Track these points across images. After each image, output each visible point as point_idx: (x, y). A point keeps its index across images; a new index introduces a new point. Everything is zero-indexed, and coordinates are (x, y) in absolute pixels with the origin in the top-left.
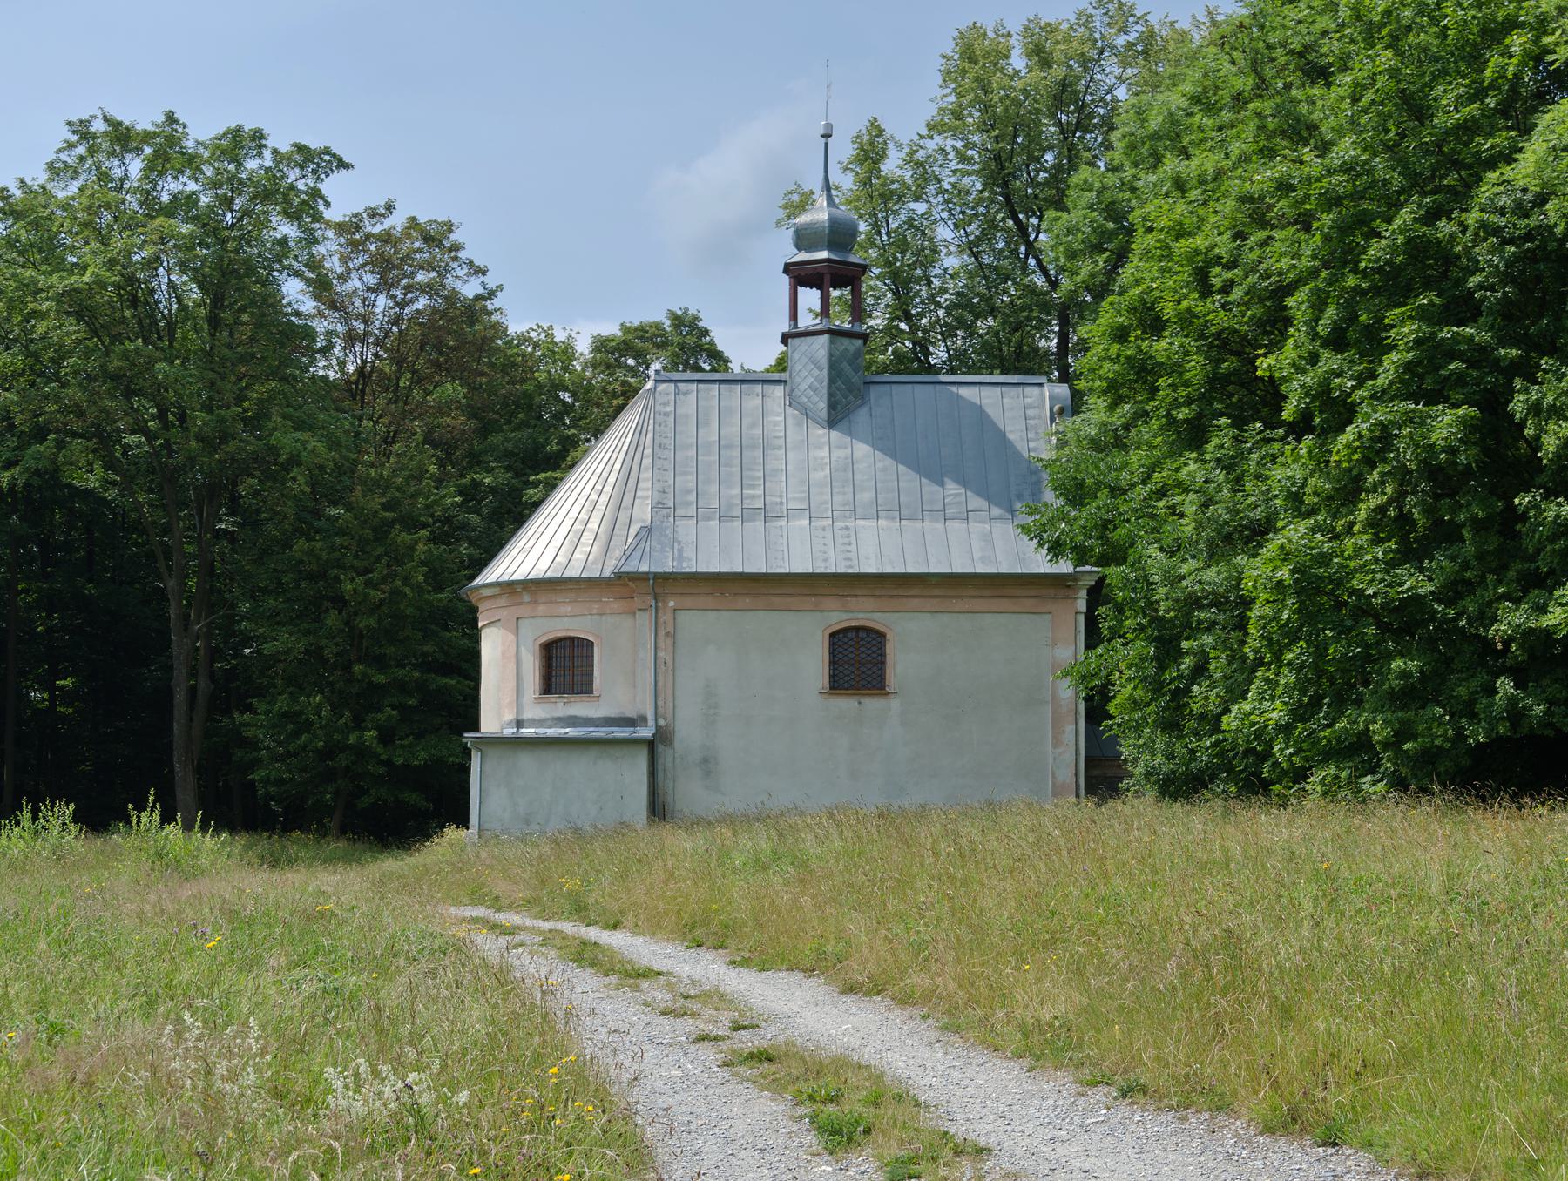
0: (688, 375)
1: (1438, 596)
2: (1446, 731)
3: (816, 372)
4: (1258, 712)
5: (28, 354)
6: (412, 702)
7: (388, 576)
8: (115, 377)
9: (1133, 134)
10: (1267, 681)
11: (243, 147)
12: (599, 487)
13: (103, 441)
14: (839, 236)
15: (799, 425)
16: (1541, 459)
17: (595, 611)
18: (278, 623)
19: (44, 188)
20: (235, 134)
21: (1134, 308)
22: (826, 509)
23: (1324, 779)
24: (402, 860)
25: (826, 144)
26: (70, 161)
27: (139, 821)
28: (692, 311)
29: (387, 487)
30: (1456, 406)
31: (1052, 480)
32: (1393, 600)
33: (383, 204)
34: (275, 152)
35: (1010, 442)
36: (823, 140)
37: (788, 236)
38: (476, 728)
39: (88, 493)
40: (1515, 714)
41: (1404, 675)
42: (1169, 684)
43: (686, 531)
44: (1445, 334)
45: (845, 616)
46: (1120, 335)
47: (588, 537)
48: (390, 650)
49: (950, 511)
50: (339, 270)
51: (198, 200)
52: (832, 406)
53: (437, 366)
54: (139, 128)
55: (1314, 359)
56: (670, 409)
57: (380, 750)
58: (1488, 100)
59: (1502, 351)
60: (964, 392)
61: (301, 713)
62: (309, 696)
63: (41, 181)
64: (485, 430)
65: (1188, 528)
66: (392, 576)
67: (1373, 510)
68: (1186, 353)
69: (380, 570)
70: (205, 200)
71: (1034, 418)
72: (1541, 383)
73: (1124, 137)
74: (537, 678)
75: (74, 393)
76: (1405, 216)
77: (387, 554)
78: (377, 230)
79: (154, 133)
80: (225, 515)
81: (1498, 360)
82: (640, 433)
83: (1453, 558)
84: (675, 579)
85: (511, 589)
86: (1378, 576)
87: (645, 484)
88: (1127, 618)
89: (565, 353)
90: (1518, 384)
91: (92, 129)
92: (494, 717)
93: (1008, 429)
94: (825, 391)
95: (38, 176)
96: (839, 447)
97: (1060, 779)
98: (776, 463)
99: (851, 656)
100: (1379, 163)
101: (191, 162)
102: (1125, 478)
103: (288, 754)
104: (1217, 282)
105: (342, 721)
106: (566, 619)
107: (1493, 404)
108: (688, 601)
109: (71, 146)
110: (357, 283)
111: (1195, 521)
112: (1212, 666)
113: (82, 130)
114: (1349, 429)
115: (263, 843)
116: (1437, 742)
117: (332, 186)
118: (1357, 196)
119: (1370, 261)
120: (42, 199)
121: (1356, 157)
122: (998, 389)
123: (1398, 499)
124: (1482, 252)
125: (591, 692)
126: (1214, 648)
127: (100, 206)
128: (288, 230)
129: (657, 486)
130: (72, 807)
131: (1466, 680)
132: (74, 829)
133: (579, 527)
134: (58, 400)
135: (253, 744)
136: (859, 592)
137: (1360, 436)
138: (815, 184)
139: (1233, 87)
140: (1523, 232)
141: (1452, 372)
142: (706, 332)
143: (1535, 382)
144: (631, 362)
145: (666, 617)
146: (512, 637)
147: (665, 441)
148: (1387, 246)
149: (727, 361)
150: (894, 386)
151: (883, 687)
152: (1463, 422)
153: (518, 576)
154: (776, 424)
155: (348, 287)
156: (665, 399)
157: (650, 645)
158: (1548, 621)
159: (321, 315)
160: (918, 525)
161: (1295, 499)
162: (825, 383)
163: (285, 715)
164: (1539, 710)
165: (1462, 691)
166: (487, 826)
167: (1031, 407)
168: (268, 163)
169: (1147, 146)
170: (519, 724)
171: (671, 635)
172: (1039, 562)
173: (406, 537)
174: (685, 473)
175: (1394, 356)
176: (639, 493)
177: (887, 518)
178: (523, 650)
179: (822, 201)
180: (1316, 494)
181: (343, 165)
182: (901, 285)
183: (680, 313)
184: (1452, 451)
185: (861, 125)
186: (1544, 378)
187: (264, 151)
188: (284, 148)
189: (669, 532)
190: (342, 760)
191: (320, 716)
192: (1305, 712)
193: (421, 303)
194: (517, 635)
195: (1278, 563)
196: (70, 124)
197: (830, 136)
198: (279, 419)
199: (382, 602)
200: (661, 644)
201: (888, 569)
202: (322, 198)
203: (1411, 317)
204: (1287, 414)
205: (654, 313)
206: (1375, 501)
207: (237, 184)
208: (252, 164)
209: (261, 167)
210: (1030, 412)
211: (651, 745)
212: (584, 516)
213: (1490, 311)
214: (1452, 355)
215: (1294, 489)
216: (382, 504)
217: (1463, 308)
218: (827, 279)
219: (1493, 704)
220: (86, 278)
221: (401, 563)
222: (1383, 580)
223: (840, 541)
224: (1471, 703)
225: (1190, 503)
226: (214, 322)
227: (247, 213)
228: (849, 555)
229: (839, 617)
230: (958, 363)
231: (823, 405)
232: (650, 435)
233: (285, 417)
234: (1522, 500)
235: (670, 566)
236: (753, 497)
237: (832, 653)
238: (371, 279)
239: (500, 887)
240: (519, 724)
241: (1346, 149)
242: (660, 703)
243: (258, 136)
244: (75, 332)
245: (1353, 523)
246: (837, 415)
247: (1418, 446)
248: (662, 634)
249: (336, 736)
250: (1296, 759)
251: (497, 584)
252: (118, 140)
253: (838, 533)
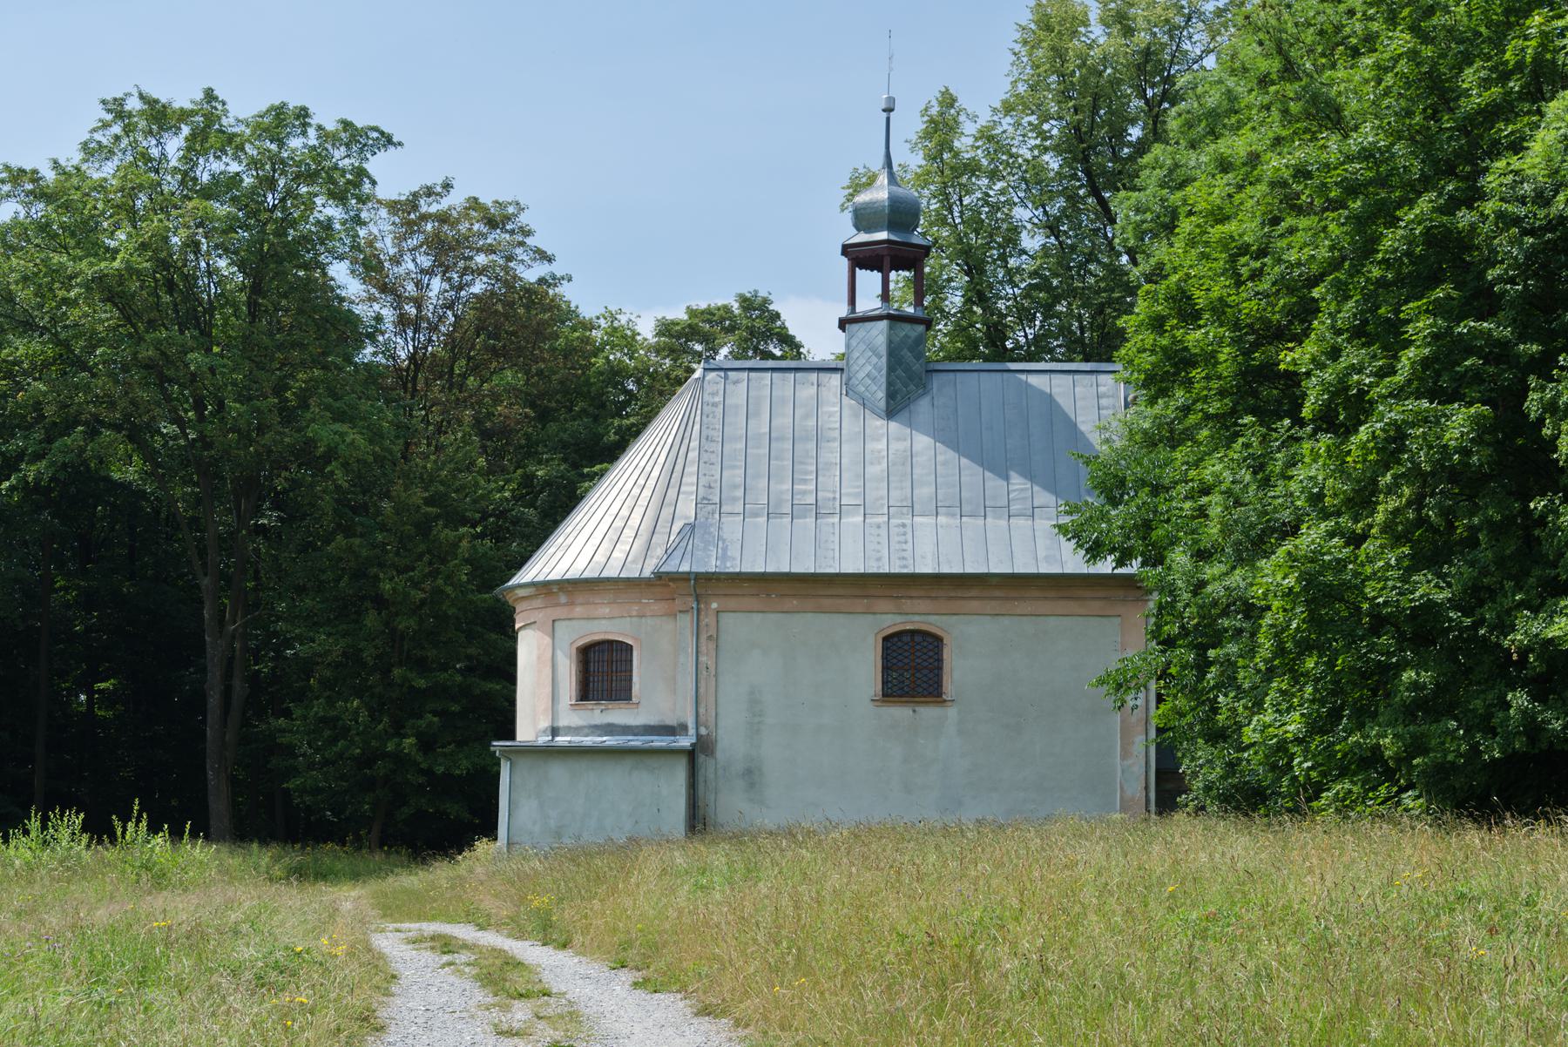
0: (757, 362)
1: (1454, 604)
2: (1460, 746)
3: (874, 360)
4: (1278, 724)
5: (57, 341)
6: (455, 708)
7: (430, 574)
8: (148, 366)
9: (1189, 112)
10: (1283, 692)
11: (286, 126)
12: (641, 481)
13: (137, 434)
14: (901, 214)
15: (856, 416)
16: (1557, 461)
17: (634, 613)
18: (315, 624)
19: (78, 169)
20: (279, 112)
21: (1172, 298)
22: (883, 505)
23: (1338, 793)
24: (416, 874)
25: (888, 120)
26: (105, 142)
27: (124, 833)
28: (763, 294)
29: (431, 481)
30: (1470, 404)
31: (1092, 477)
32: (1404, 609)
33: (440, 182)
34: (320, 128)
35: (1082, 433)
36: (885, 115)
37: (848, 217)
38: (511, 735)
39: (124, 486)
40: (1532, 728)
41: (1415, 686)
42: (1208, 693)
43: (732, 528)
44: (1461, 329)
45: (899, 619)
46: (1157, 323)
47: (629, 533)
48: (431, 653)
49: (1014, 508)
50: (392, 251)
51: (242, 181)
52: (891, 395)
53: (494, 351)
54: (176, 105)
55: (1335, 353)
56: (719, 399)
57: (419, 758)
58: (1511, 84)
59: (1522, 347)
60: (1034, 380)
61: (338, 718)
62: (346, 702)
63: (75, 162)
64: (544, 416)
65: (1213, 529)
66: (434, 574)
67: (1391, 513)
68: (1220, 344)
69: (422, 568)
70: (248, 181)
71: (1107, 408)
72: (1559, 381)
73: (1180, 115)
74: (574, 684)
75: (101, 385)
76: (1424, 204)
77: (429, 551)
78: (434, 209)
79: (192, 111)
80: (270, 509)
81: (1518, 356)
82: (686, 424)
83: (1472, 564)
84: (718, 580)
85: (547, 589)
86: (1390, 583)
87: (690, 479)
88: (1166, 624)
89: (625, 339)
90: (1533, 381)
91: (127, 108)
92: (530, 726)
93: (1079, 419)
94: (884, 380)
95: (71, 156)
96: (898, 439)
97: (1129, 793)
98: (830, 455)
99: (906, 661)
100: (1400, 148)
101: (230, 143)
102: (1169, 475)
103: (326, 762)
104: (1245, 272)
105: (380, 727)
106: (604, 622)
107: (1508, 401)
108: (732, 603)
109: (106, 125)
110: (411, 266)
111: (1221, 523)
112: (1241, 674)
113: (117, 109)
114: (1362, 429)
115: (294, 857)
116: (1450, 757)
117: (377, 164)
118: (1382, 182)
119: (1386, 252)
120: (75, 181)
121: (1375, 143)
122: (1070, 377)
123: (1417, 502)
124: (1502, 242)
125: (629, 698)
126: (1241, 656)
127: (133, 188)
128: (333, 212)
129: (703, 481)
130: (82, 815)
131: (1483, 692)
132: (85, 838)
133: (619, 523)
134: (87, 388)
135: (289, 750)
136: (914, 593)
137: (1374, 437)
138: (877, 163)
139: (1258, 69)
140: (1544, 222)
141: (1468, 369)
142: (778, 316)
143: (1551, 380)
144: (698, 347)
145: (709, 619)
146: (548, 640)
147: (711, 433)
148: (1402, 237)
149: (798, 346)
150: (958, 374)
151: (940, 695)
152: (1476, 420)
153: (554, 576)
154: (831, 415)
155: (401, 270)
156: (715, 388)
157: (691, 649)
158: (1552, 632)
159: (372, 299)
160: (980, 521)
161: (1316, 499)
162: (884, 372)
163: (323, 720)
164: (1557, 725)
165: (1477, 704)
166: (516, 839)
167: (1105, 396)
168: (313, 141)
169: (1203, 124)
170: (555, 731)
171: (715, 639)
172: (1072, 561)
173: (447, 534)
174: (734, 467)
175: (1411, 352)
176: (683, 489)
177: (948, 515)
178: (559, 654)
179: (883, 179)
180: (1335, 495)
181: (388, 141)
182: (974, 267)
183: (748, 295)
184: (1465, 452)
185: (932, 95)
186: (1560, 376)
187: (309, 130)
188: (331, 126)
189: (714, 530)
190: (381, 768)
191: (357, 722)
192: (1325, 724)
193: (478, 288)
194: (553, 638)
195: (1287, 570)
196: (104, 102)
197: (892, 110)
198: (317, 410)
199: (423, 602)
200: (703, 649)
201: (945, 570)
202: (369, 177)
203: (1427, 311)
204: (1306, 413)
205: (725, 297)
206: (1393, 503)
207: (278, 162)
208: (295, 143)
209: (305, 146)
210: (1104, 402)
211: (691, 754)
212: (624, 512)
213: (1512, 303)
214: (1470, 351)
215: (1315, 490)
216: (425, 499)
217: (1483, 302)
218: (887, 262)
219: (1508, 718)
220: (116, 264)
221: (444, 561)
222: (1394, 588)
223: (895, 539)
224: (1489, 716)
225: (1215, 504)
226: (254, 310)
227: (289, 193)
228: (904, 554)
229: (892, 621)
230: (1037, 350)
231: (881, 395)
232: (697, 427)
233: (328, 408)
234: (1538, 505)
235: (712, 566)
236: (804, 493)
238: (425, 261)
239: (488, 904)
240: (555, 731)
241: (1367, 135)
242: (702, 711)
243: (303, 114)
244: (108, 319)
245: (1371, 526)
246: (897, 404)
247: (1431, 447)
248: (703, 637)
249: (373, 743)
250: (1313, 774)
251: (533, 584)
252: (155, 118)
253: (894, 530)
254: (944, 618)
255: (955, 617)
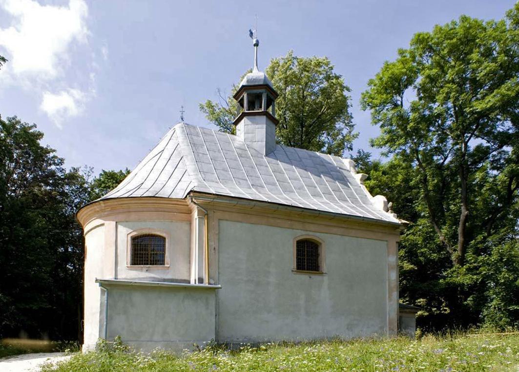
45: (304, 233)
229: (302, 234)
237: (298, 251)
254: (322, 234)
255: (329, 235)
